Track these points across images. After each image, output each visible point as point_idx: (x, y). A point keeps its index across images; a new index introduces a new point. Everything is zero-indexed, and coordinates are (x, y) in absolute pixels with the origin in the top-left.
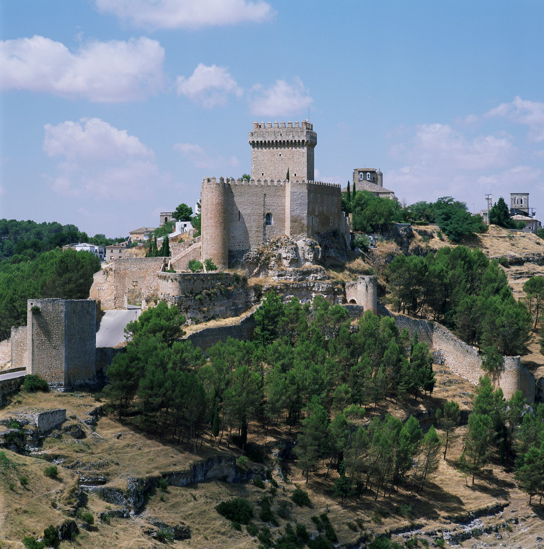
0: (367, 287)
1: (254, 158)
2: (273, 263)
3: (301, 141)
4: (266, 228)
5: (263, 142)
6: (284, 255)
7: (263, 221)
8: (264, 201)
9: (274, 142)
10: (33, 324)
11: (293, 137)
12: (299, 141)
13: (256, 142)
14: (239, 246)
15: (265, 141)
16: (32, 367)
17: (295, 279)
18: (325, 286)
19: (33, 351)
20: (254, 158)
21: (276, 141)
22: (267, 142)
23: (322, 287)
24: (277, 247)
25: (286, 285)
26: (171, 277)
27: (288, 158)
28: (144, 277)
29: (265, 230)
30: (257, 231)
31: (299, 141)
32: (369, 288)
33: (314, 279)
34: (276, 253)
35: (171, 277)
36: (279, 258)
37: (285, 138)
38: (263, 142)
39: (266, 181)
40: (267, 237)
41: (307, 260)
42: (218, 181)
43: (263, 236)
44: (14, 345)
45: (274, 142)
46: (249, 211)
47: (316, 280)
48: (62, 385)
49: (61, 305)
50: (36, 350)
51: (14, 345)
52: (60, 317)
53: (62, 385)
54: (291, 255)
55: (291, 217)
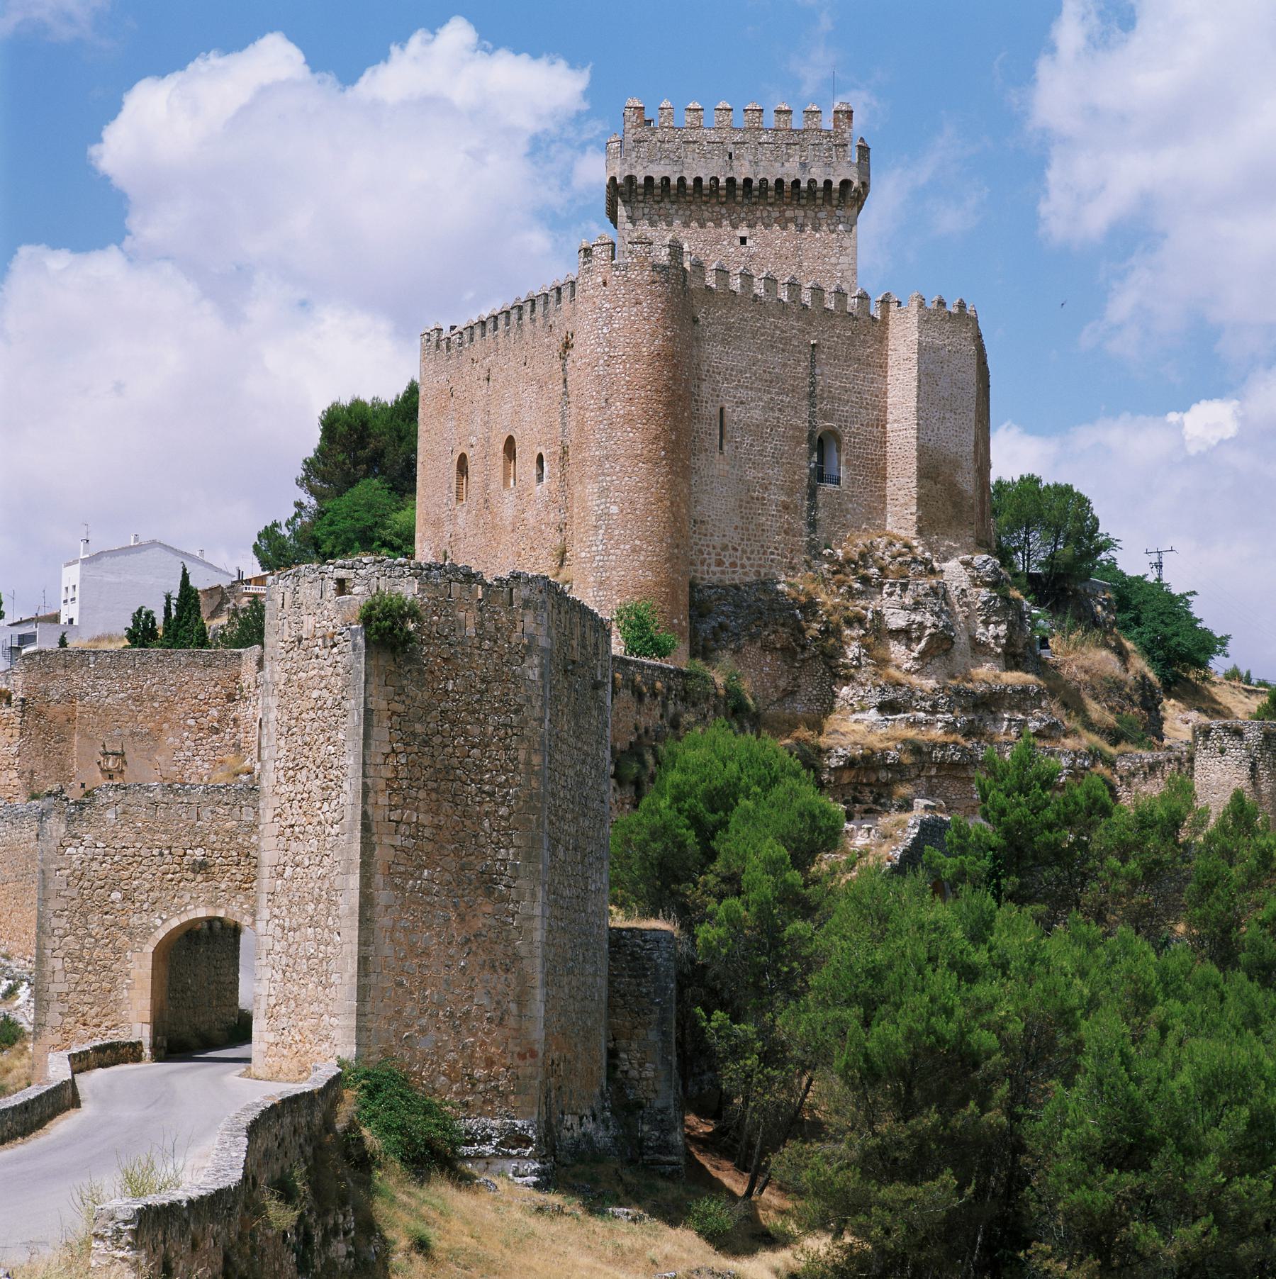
0: (1253, 768)
2: (853, 650)
3: (836, 185)
4: (820, 497)
5: (674, 181)
6: (897, 620)
7: (805, 468)
8: (813, 375)
9: (722, 182)
10: (368, 714)
11: (803, 165)
12: (828, 183)
13: (641, 181)
14: (720, 563)
15: (681, 180)
16: (360, 1015)
17: (950, 728)
19: (366, 901)
21: (731, 181)
22: (690, 182)
24: (865, 580)
25: (916, 749)
27: (778, 255)
28: (155, 736)
30: (786, 507)
32: (1264, 773)
34: (865, 607)
36: (878, 632)
37: (771, 170)
38: (674, 181)
40: (821, 536)
41: (978, 648)
42: (663, 256)
43: (806, 529)
44: (54, 904)
45: (722, 182)
46: (757, 415)
48: (524, 1141)
49: (527, 603)
50: (383, 896)
51: (54, 904)
52: (517, 679)
53: (524, 1141)
54: (929, 620)
55: (922, 452)
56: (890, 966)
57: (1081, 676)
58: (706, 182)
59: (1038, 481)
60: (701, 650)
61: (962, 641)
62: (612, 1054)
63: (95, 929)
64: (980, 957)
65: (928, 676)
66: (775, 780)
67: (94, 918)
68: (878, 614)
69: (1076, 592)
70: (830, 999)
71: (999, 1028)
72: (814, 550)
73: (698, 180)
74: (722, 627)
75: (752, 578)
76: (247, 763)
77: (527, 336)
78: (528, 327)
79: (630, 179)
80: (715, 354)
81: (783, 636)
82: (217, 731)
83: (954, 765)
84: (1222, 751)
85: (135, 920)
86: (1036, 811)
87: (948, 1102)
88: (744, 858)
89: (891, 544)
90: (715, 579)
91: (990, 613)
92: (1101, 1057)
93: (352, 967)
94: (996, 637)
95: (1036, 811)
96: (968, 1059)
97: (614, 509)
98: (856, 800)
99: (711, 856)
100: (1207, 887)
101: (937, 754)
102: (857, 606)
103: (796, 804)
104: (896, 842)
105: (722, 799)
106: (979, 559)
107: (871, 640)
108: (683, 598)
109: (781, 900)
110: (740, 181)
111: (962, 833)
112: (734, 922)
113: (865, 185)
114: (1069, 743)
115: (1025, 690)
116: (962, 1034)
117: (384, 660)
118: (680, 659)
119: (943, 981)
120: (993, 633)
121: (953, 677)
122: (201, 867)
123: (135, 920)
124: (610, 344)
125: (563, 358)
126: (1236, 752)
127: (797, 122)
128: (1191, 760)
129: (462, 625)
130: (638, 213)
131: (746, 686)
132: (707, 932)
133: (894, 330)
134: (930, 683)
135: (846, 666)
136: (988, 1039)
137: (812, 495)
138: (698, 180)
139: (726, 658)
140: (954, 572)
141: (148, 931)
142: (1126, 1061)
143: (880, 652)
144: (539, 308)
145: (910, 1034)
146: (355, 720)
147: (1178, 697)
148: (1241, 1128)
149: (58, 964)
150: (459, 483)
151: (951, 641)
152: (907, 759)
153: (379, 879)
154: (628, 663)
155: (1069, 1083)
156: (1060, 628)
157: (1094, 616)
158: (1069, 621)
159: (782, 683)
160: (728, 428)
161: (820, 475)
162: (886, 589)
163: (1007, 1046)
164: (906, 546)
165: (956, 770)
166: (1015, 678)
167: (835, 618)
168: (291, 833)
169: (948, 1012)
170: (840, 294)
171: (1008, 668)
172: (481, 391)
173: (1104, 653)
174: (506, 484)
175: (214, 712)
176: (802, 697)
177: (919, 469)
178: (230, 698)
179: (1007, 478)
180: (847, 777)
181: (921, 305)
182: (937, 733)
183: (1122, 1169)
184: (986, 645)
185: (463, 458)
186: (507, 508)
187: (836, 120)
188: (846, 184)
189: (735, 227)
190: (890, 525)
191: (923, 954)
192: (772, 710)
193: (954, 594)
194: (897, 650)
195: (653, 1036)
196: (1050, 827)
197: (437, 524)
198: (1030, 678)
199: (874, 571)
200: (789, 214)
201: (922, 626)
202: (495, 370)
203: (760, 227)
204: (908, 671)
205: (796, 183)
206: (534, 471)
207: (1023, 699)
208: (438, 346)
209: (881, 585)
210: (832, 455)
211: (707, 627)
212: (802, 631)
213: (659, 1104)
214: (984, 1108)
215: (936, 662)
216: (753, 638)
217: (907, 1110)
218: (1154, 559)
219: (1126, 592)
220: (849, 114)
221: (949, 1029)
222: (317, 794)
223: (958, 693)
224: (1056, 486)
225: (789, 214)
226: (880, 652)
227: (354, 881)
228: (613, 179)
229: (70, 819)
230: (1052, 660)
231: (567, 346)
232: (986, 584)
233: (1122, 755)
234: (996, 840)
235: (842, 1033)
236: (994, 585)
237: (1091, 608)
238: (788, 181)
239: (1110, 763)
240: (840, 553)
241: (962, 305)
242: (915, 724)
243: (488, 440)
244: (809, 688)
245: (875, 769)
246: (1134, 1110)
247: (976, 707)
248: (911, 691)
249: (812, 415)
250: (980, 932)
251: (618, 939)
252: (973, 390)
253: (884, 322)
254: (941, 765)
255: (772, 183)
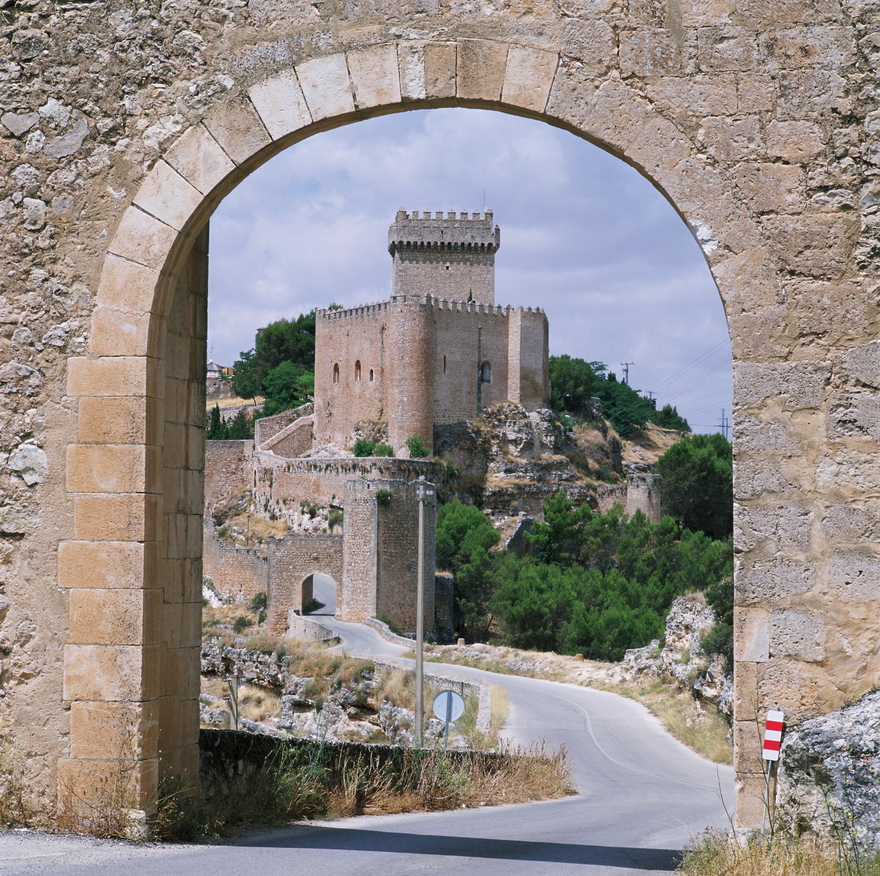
0: (649, 493)
1: (401, 271)
2: (495, 449)
3: (486, 245)
4: (482, 387)
5: (419, 243)
6: (512, 436)
7: (476, 375)
8: (479, 340)
9: (439, 244)
10: (378, 523)
11: (473, 237)
12: (483, 244)
13: (405, 243)
14: (444, 416)
15: (422, 243)
16: (377, 605)
17: (532, 479)
18: (576, 491)
19: (378, 573)
20: (401, 271)
21: (443, 243)
22: (425, 244)
23: (571, 494)
24: (499, 420)
25: (519, 487)
26: (379, 464)
29: (479, 392)
31: (483, 244)
32: (654, 495)
33: (557, 479)
34: (499, 431)
35: (379, 464)
36: (505, 441)
37: (459, 239)
38: (419, 243)
39: (481, 306)
40: (482, 404)
41: (543, 445)
42: (424, 301)
44: (273, 569)
45: (439, 244)
46: (458, 358)
47: (560, 480)
50: (382, 573)
54: (524, 436)
55: (522, 369)
56: (519, 589)
57: (586, 445)
58: (432, 244)
59: (569, 357)
60: (438, 452)
61: (537, 443)
62: (436, 613)
63: (285, 577)
64: (544, 586)
65: (524, 458)
66: (478, 523)
67: (285, 573)
68: (504, 434)
69: (585, 405)
70: (501, 598)
71: (549, 607)
72: (480, 409)
73: (429, 243)
74: (445, 442)
75: (456, 422)
76: (248, 487)
77: (366, 321)
78: (366, 318)
79: (401, 242)
80: (441, 335)
81: (467, 444)
82: (234, 473)
83: (533, 493)
84: (638, 486)
85: (296, 574)
86: (564, 519)
87: (535, 628)
88: (471, 550)
89: (509, 406)
90: (442, 423)
91: (548, 431)
92: (578, 615)
93: (375, 592)
94: (550, 441)
95: (564, 519)
96: (540, 616)
97: (405, 399)
98: (496, 508)
99: (459, 548)
100: (625, 547)
101: (527, 489)
102: (496, 431)
103: (486, 533)
104: (513, 528)
105: (462, 530)
106: (544, 410)
107: (501, 444)
108: (431, 432)
109: (483, 565)
110: (446, 243)
111: (537, 526)
112: (468, 571)
113: (498, 245)
114: (578, 483)
115: (561, 463)
116: (539, 609)
117: (382, 508)
118: (430, 459)
119: (534, 594)
120: (549, 440)
121: (533, 458)
122: (316, 559)
123: (296, 574)
124: (404, 335)
125: (382, 333)
126: (643, 487)
127: (470, 217)
128: (626, 489)
129: (402, 497)
130: (404, 256)
131: (455, 466)
132: (459, 574)
133: (512, 320)
134: (524, 461)
135: (492, 455)
136: (546, 610)
137: (479, 388)
138: (429, 243)
139: (446, 453)
140: (534, 417)
141: (300, 578)
142: (584, 616)
143: (505, 449)
144: (371, 310)
145: (525, 609)
146: (375, 524)
147: (631, 439)
148: (616, 634)
149: (273, 587)
150: (335, 375)
151: (533, 444)
152: (515, 491)
153: (381, 568)
154: (413, 462)
155: (569, 622)
156: (578, 422)
157: (592, 414)
158: (580, 419)
159: (467, 462)
160: (447, 363)
161: (482, 380)
162: (508, 424)
163: (551, 611)
164: (516, 406)
165: (535, 495)
166: (558, 458)
167: (488, 436)
168: (353, 554)
169: (535, 603)
170: (491, 307)
171: (556, 453)
172: (345, 340)
173: (596, 432)
174: (356, 379)
175: (233, 466)
176: (475, 467)
177: (521, 376)
178: (240, 460)
179: (556, 356)
180: (492, 499)
181: (522, 310)
182: (527, 481)
183: (583, 646)
184: (546, 444)
185: (336, 365)
186: (357, 388)
187: (486, 217)
188: (490, 244)
189: (444, 263)
190: (510, 397)
191: (528, 586)
192: (463, 473)
193: (534, 425)
194: (512, 448)
195: (447, 608)
196: (569, 525)
197: (325, 390)
198: (564, 457)
199: (503, 417)
200: (466, 257)
201: (521, 439)
202: (351, 332)
203: (455, 263)
204: (516, 456)
205: (470, 244)
206: (369, 376)
207: (560, 465)
208: (324, 317)
209: (505, 422)
210: (487, 371)
211: (439, 442)
212: (475, 442)
213: (449, 628)
214: (545, 629)
215: (527, 453)
216: (456, 445)
217: (523, 630)
218: (624, 367)
219: (609, 391)
220: (491, 214)
221: (535, 607)
222: (362, 544)
223: (535, 464)
224: (577, 359)
225: (466, 257)
226: (505, 449)
227: (375, 569)
228: (394, 242)
229: (277, 545)
230: (574, 437)
231: (383, 329)
232: (546, 421)
233: (600, 486)
234: (550, 529)
235: (506, 608)
236: (549, 421)
237: (591, 410)
238: (466, 243)
239: (595, 490)
240: (490, 410)
241: (538, 309)
242: (519, 477)
243: (348, 360)
244: (477, 463)
245: (503, 495)
246: (587, 631)
247: (542, 469)
248: (517, 465)
249: (479, 355)
250: (544, 577)
251: (438, 579)
252: (542, 343)
253: (507, 317)
254: (528, 493)
255: (459, 244)
